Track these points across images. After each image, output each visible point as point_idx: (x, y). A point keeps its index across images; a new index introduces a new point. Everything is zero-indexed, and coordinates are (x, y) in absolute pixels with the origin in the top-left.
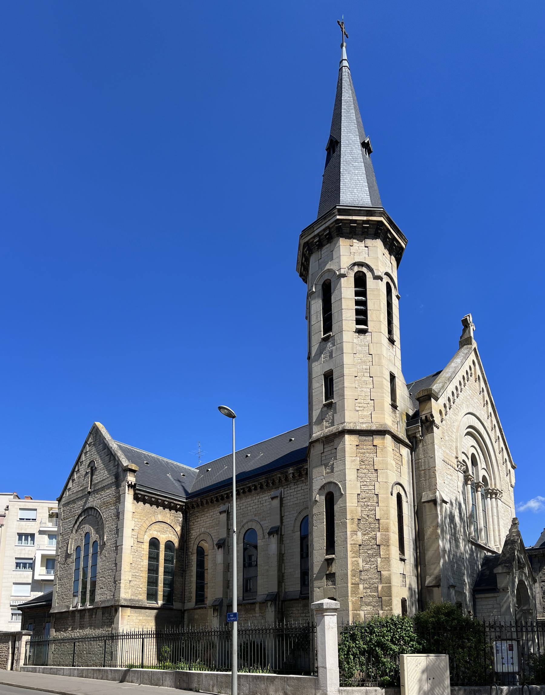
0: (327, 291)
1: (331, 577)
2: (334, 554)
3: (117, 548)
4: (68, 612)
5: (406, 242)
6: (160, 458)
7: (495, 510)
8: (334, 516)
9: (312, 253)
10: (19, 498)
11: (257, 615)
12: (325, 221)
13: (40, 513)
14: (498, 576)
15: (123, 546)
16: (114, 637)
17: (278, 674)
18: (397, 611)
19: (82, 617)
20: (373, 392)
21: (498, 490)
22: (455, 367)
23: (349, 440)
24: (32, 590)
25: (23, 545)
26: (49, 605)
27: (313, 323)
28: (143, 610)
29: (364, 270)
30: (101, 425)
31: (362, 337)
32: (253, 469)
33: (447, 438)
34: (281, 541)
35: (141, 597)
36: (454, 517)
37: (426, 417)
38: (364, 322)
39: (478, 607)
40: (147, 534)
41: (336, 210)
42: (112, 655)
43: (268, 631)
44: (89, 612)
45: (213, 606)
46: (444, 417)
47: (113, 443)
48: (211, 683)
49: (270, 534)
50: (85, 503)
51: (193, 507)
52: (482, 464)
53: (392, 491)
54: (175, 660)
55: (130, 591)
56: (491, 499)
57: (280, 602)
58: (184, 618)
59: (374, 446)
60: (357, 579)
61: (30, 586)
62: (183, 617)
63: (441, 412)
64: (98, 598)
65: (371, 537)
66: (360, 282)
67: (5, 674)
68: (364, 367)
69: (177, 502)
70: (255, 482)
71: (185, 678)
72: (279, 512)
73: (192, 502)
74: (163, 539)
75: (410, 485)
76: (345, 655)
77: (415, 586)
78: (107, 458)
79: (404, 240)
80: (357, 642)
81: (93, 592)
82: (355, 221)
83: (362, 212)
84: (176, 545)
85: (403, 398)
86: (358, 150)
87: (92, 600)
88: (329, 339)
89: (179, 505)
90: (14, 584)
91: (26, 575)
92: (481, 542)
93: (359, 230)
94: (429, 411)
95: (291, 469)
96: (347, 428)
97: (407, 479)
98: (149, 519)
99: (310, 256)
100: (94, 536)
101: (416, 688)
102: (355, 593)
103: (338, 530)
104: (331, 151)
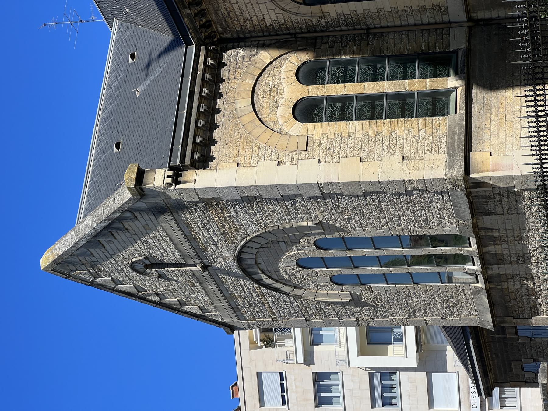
3: (327, 194)
6: (99, 116)
15: (321, 181)
19: (500, 260)
24: (443, 369)
25: (341, 394)
26: (477, 332)
28: (475, 121)
30: (45, 256)
40: (285, 129)
44: (486, 246)
47: (82, 226)
50: (230, 274)
51: (207, 25)
55: (428, 157)
58: (491, 19)
61: (435, 375)
62: (488, 22)
69: (201, 67)
74: (293, 91)
78: (121, 236)
87: (457, 240)
100: (305, 249)
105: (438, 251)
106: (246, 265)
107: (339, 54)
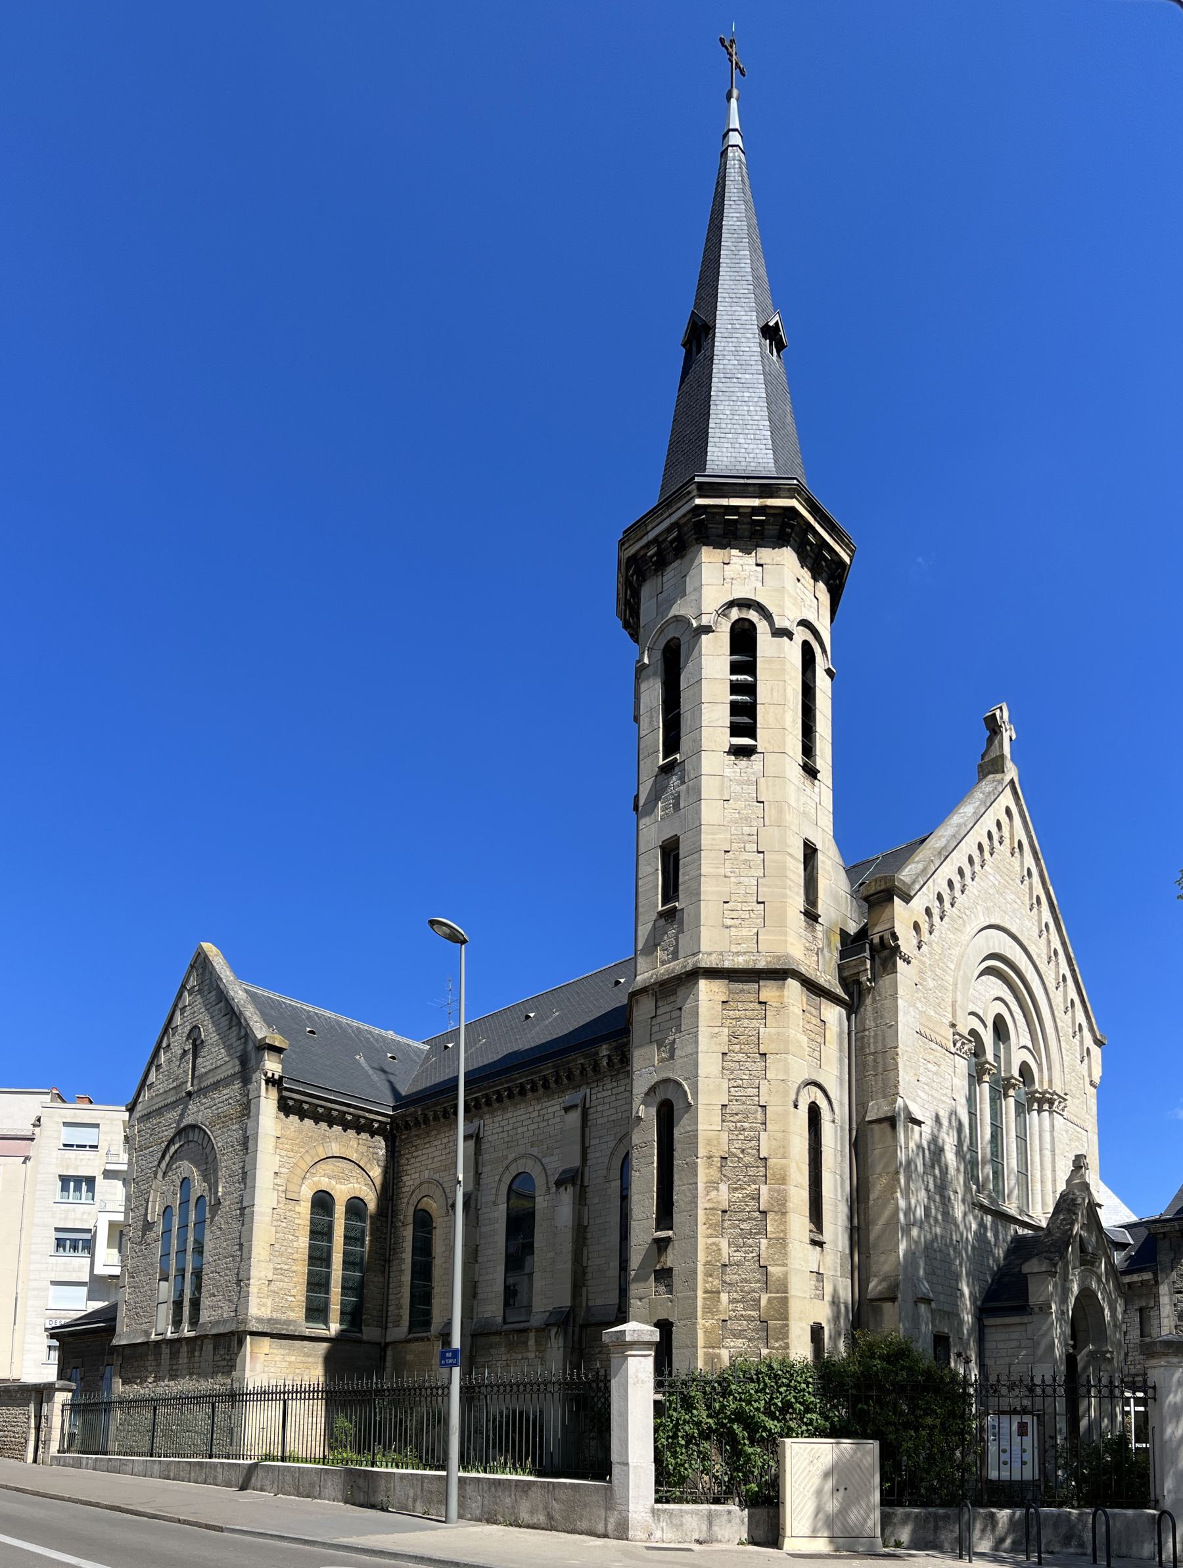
0: (673, 662)
1: (664, 1276)
2: (671, 1229)
3: (244, 1212)
4: (147, 1343)
5: (852, 551)
6: (344, 1019)
7: (1047, 1137)
8: (673, 1150)
9: (644, 580)
10: (64, 1101)
11: (531, 1355)
12: (670, 511)
13: (106, 1133)
14: (1030, 1279)
15: (256, 1208)
16: (236, 1397)
17: (539, 1476)
18: (801, 1350)
19: (174, 1355)
20: (764, 885)
21: (1055, 1093)
22: (959, 826)
23: (708, 992)
24: (90, 1298)
25: (71, 1200)
26: (111, 1330)
27: (643, 733)
28: (297, 1343)
29: (753, 615)
30: (214, 948)
31: (743, 763)
32: (533, 1045)
33: (931, 984)
34: (581, 1199)
35: (292, 1315)
36: (942, 1150)
37: (881, 938)
38: (750, 731)
39: (989, 1345)
40: (307, 1182)
41: (694, 486)
42: (233, 1434)
43: (535, 1387)
44: (187, 1344)
45: (442, 1335)
46: (925, 936)
47: (237, 988)
48: (411, 1494)
49: (559, 1183)
50: (182, 1116)
51: (407, 1127)
52: (1019, 1035)
53: (797, 1100)
54: (363, 1445)
55: (269, 1302)
56: (1039, 1113)
57: (577, 1329)
58: (385, 1361)
59: (760, 1003)
60: (716, 1282)
61: (85, 1289)
62: (383, 1358)
63: (916, 927)
64: (205, 1316)
65: (748, 1196)
66: (743, 641)
67: (17, 1471)
68: (747, 830)
69: (372, 1116)
70: (532, 1074)
71: (361, 1482)
72: (578, 1138)
73: (405, 1116)
74: (342, 1192)
75: (841, 1084)
76: (669, 1437)
77: (846, 1295)
78: (224, 1022)
79: (847, 545)
80: (695, 1412)
81: (196, 1304)
82: (735, 509)
83: (751, 489)
84: (372, 1206)
85: (836, 898)
86: (752, 344)
87: (194, 1322)
88: (673, 768)
89: (377, 1121)
90: (53, 1283)
91: (77, 1266)
92: (1011, 1208)
93: (744, 529)
94: (888, 926)
95: (604, 1047)
96: (703, 965)
97: (836, 1072)
98: (312, 1152)
99: (640, 586)
100: (198, 1186)
101: (810, 1507)
102: (710, 1310)
103: (681, 1179)
104: (694, 349)
105: (186, 1303)
106: (186, 1132)
107: (371, 1235)
